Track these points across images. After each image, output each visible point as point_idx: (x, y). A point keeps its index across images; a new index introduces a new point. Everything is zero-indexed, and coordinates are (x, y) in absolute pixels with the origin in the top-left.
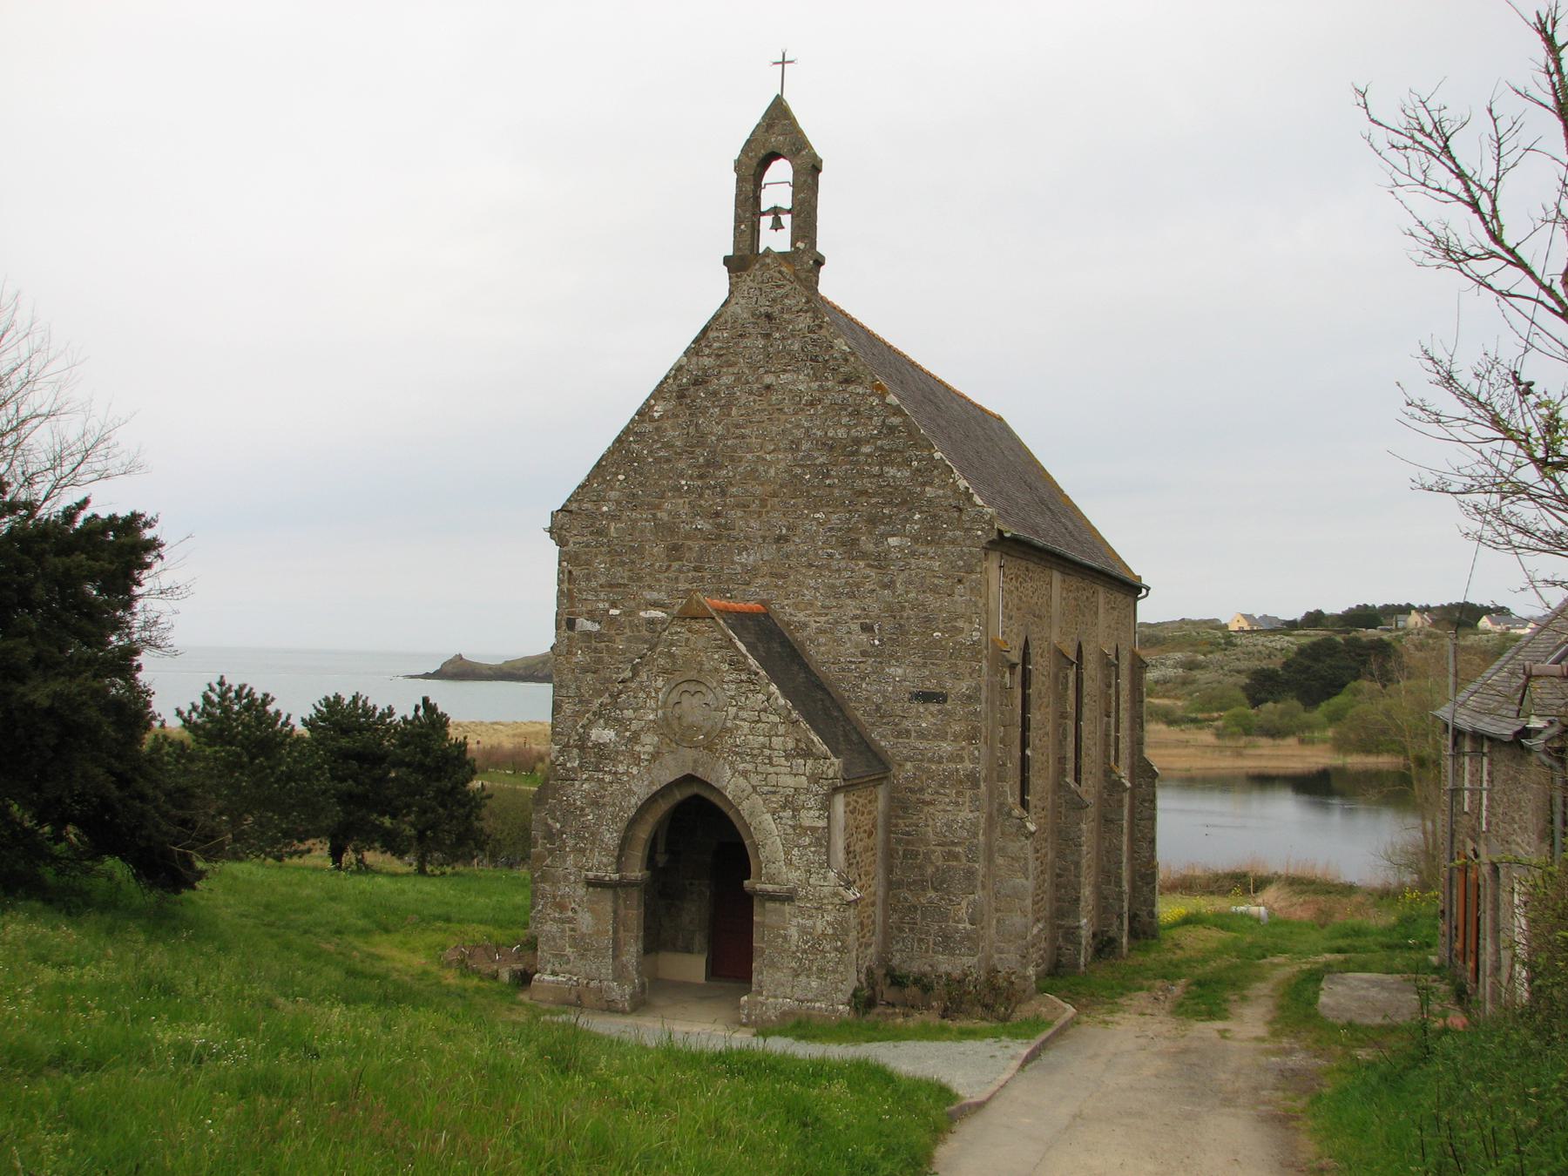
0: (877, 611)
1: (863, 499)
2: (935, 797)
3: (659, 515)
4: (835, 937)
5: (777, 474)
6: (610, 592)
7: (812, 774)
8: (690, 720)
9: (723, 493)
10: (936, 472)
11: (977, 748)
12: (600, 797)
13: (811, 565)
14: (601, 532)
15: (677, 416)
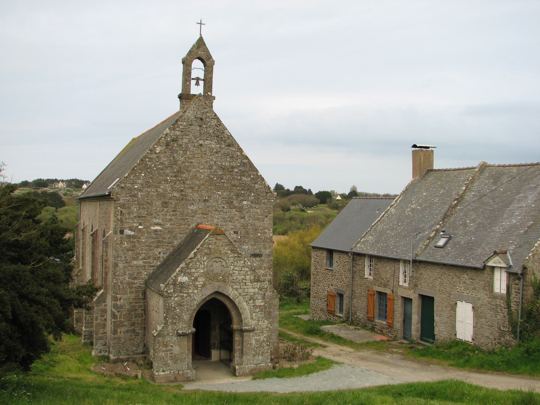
1: (235, 188)
3: (159, 190)
4: (267, 341)
5: (204, 177)
6: (139, 220)
7: (260, 288)
8: (216, 272)
9: (184, 183)
10: (258, 180)
13: (217, 210)
14: (135, 196)
15: (166, 153)
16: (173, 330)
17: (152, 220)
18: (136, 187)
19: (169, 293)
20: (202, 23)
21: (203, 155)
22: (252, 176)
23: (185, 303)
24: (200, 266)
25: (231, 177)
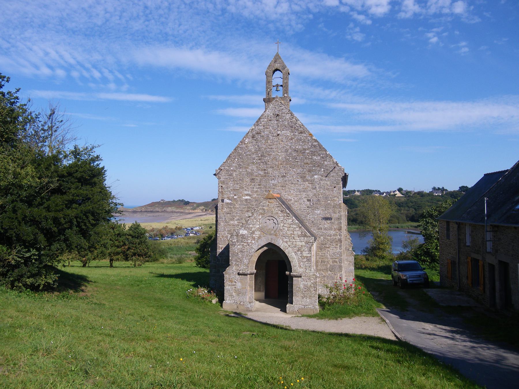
0: (312, 195)
1: (307, 165)
3: (248, 170)
7: (306, 241)
10: (327, 158)
13: (292, 183)
14: (231, 175)
18: (232, 169)
23: (245, 250)
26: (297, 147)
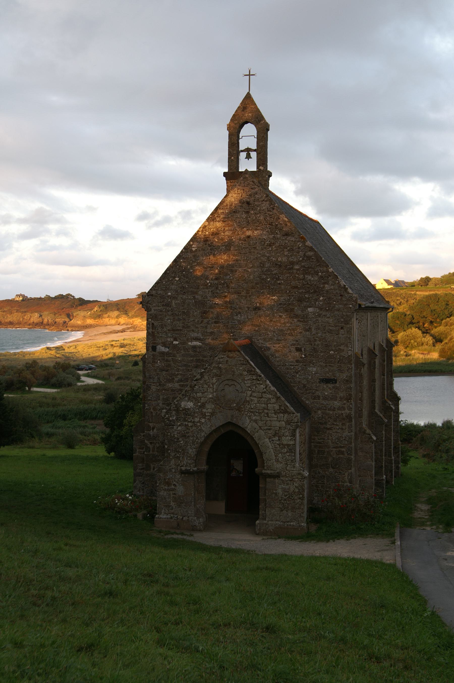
1: (296, 290)
2: (332, 426)
3: (196, 297)
7: (287, 421)
10: (330, 278)
11: (351, 404)
12: (187, 433)
14: (168, 305)
16: (175, 465)
17: (189, 334)
18: (169, 294)
19: (171, 421)
20: (251, 74)
21: (252, 250)
22: (320, 274)
24: (208, 389)
25: (291, 276)
26: (279, 259)
